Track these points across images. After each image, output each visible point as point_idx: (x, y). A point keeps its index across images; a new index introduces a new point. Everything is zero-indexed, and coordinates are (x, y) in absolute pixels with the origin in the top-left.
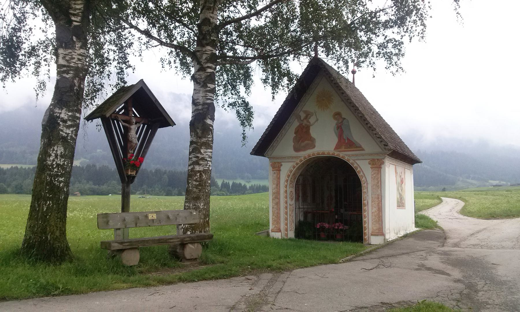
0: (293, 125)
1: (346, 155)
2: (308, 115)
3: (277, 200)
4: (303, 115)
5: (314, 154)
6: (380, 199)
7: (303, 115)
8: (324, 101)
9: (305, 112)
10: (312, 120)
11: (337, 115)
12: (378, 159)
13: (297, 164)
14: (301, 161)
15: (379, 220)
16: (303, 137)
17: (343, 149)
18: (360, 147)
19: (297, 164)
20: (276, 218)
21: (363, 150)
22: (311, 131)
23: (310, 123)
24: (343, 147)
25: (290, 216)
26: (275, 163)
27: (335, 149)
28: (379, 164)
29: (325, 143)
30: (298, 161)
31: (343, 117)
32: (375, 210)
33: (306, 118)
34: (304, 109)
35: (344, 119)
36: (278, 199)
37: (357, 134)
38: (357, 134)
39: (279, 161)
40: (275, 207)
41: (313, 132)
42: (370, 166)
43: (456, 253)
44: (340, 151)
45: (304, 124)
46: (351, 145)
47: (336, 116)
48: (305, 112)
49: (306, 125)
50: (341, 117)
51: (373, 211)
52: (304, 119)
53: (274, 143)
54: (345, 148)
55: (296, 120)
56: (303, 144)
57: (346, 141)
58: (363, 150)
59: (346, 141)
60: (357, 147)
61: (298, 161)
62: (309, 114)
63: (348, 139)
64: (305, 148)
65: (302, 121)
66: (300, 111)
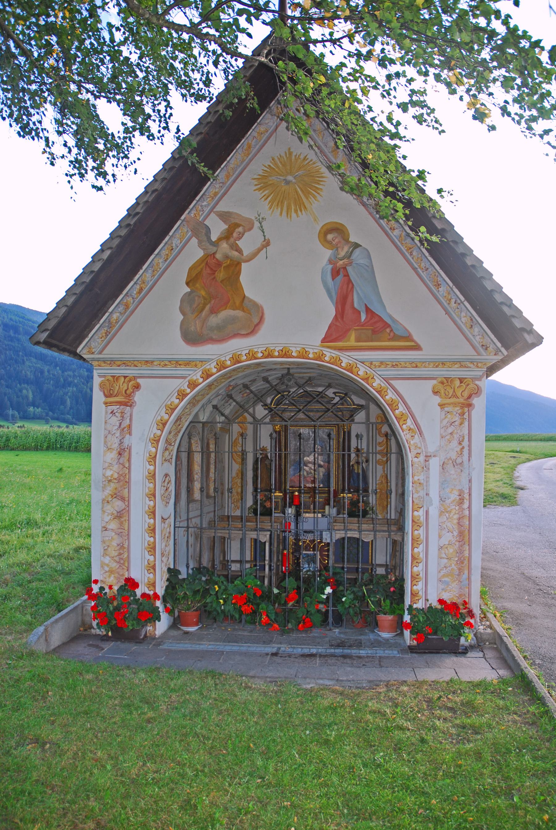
0: (181, 253)
1: (359, 362)
2: (234, 227)
3: (118, 504)
4: (217, 228)
5: (252, 355)
6: (466, 505)
7: (217, 228)
8: (288, 189)
9: (224, 216)
10: (248, 243)
11: (334, 233)
12: (461, 380)
13: (193, 385)
14: (207, 375)
15: (460, 570)
16: (217, 288)
17: (352, 342)
18: (409, 337)
19: (193, 385)
20: (114, 565)
21: (417, 347)
22: (243, 279)
23: (240, 251)
24: (353, 336)
25: (163, 555)
26: (116, 378)
27: (323, 341)
28: (466, 394)
29: (292, 323)
30: (197, 376)
31: (353, 239)
32: (448, 538)
33: (227, 236)
34: (221, 207)
35: (357, 246)
36: (123, 499)
37: (399, 286)
38: (399, 286)
39: (131, 372)
40: (113, 525)
41: (252, 282)
42: (437, 400)
43: (274, 565)
44: (341, 349)
45: (219, 256)
46: (379, 329)
47: (330, 237)
48: (224, 216)
49: (227, 257)
50: (347, 241)
51: (444, 541)
52: (220, 239)
53: (114, 311)
54: (358, 340)
55: (194, 241)
56: (214, 320)
57: (363, 317)
58: (417, 347)
59: (363, 317)
60: (396, 338)
61: (197, 376)
62: (237, 225)
63: (368, 310)
64: (222, 335)
65: (215, 244)
66: (208, 211)
